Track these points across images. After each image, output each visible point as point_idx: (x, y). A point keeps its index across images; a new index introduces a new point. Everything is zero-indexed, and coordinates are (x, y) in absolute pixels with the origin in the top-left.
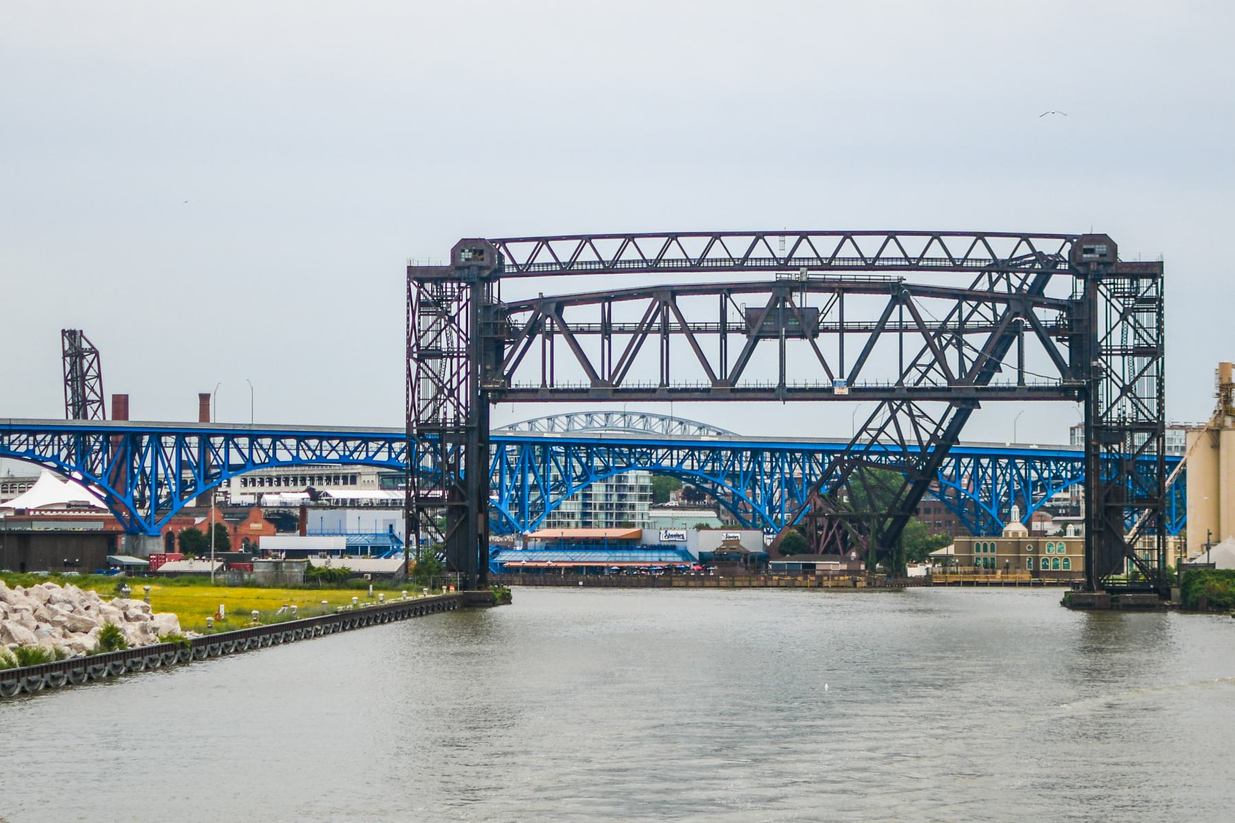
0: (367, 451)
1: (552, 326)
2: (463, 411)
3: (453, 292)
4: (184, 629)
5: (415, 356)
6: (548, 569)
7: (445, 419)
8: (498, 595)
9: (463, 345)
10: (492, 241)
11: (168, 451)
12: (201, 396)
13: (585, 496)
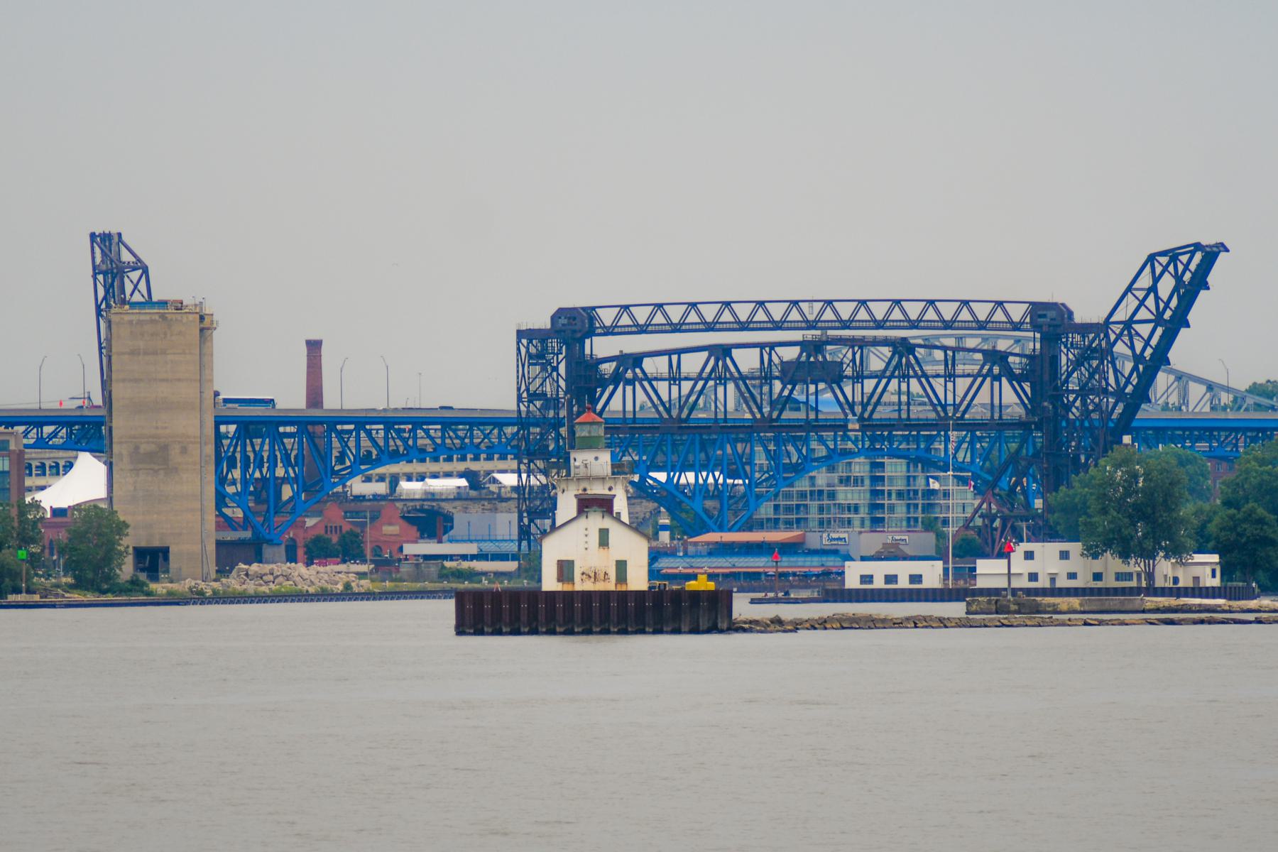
12: (309, 343)
13: (876, 480)
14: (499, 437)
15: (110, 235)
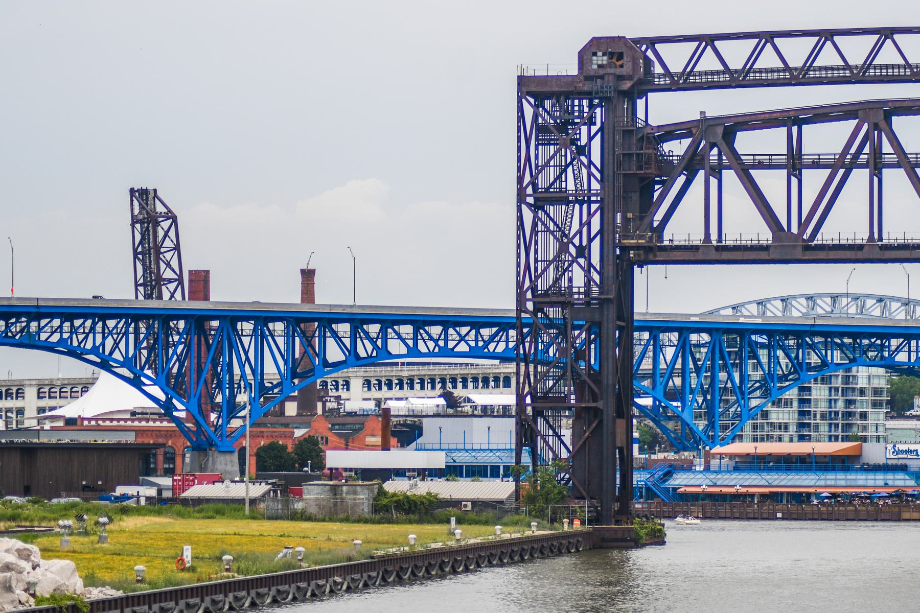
0: (507, 341)
1: (720, 159)
2: (596, 277)
3: (581, 111)
4: (91, 581)
5: (530, 200)
6: (736, 496)
7: (570, 287)
8: (642, 533)
9: (595, 186)
10: (638, 41)
11: (246, 340)
12: (303, 272)
13: (802, 401)
14: (476, 341)
15: (147, 190)
